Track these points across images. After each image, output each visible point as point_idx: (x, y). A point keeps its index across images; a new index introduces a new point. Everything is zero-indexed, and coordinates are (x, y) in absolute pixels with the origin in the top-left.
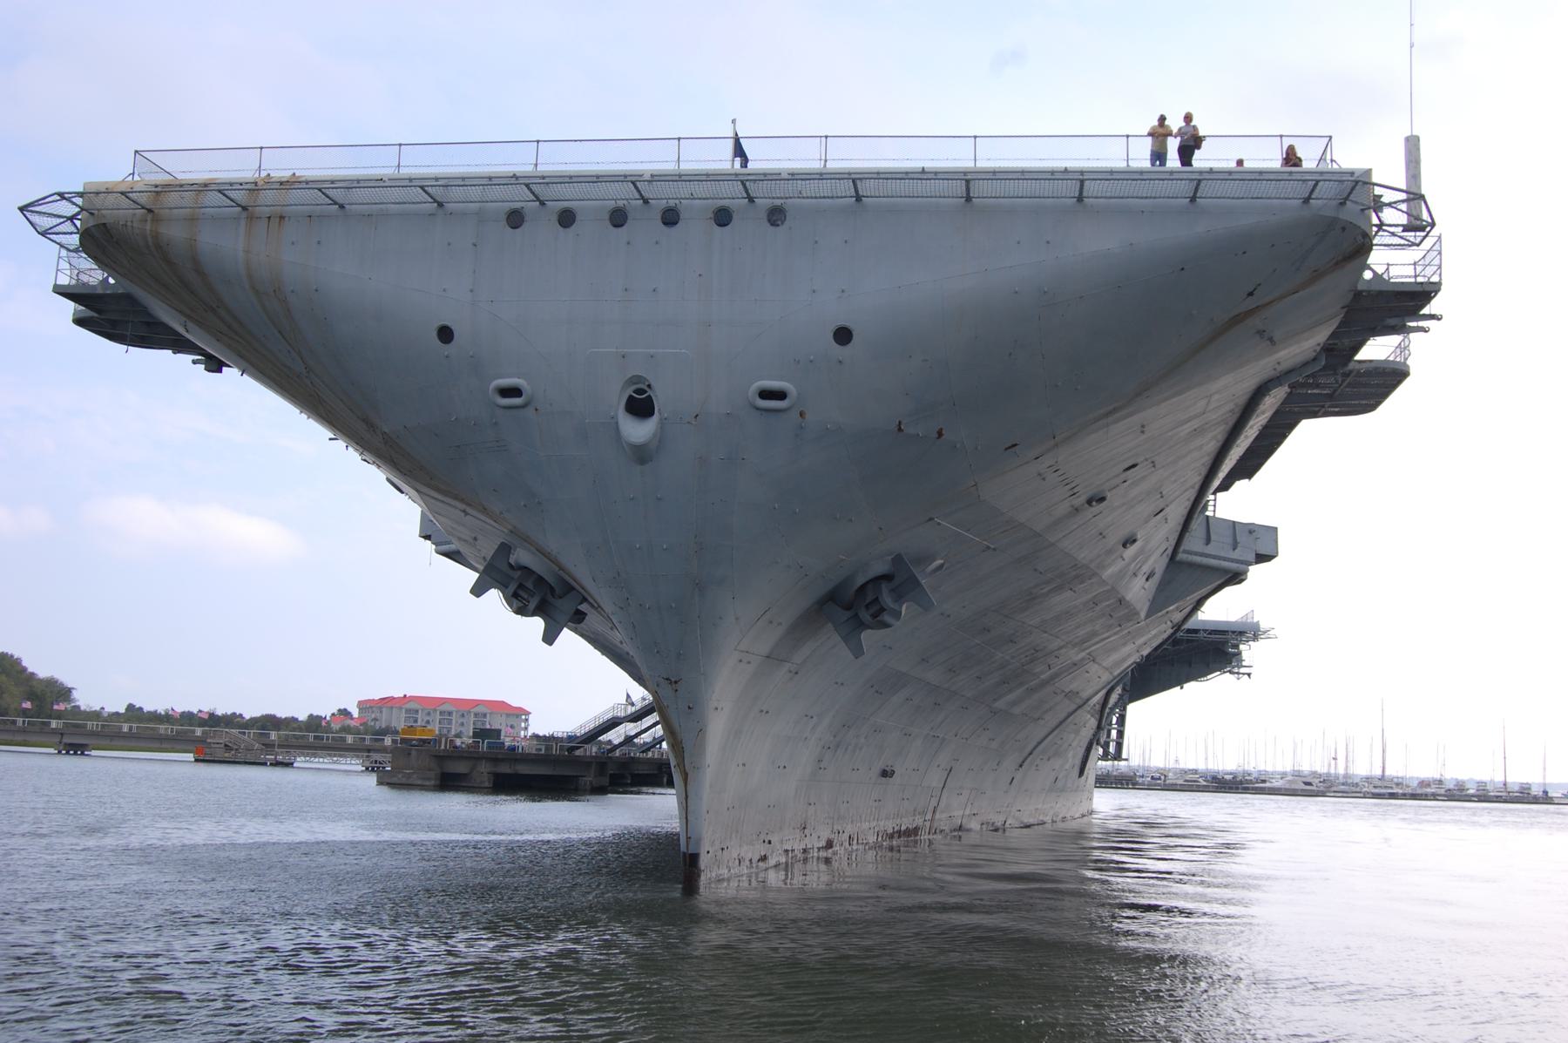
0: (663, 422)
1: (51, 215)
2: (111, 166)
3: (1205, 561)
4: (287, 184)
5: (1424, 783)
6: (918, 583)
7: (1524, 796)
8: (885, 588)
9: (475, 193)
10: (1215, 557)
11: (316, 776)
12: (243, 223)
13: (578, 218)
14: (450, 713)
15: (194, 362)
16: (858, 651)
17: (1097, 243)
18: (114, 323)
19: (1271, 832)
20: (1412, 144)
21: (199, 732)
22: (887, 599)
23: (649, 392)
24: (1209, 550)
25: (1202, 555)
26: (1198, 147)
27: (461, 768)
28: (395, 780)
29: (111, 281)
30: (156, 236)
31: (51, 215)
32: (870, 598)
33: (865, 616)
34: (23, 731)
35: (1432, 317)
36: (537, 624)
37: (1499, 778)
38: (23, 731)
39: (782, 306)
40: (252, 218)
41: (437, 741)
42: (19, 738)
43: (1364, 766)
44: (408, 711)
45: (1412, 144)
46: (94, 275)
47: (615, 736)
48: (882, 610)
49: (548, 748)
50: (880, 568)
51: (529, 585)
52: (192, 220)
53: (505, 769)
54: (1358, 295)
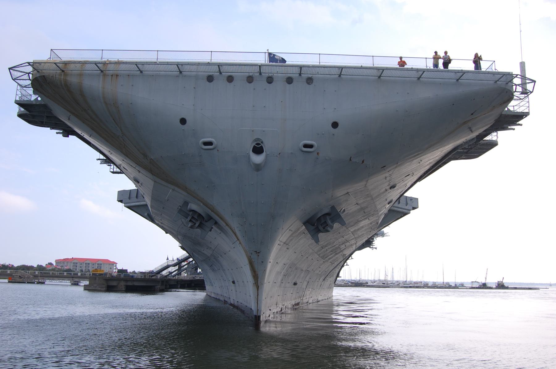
1: (21, 72)
2: (42, 55)
4: (118, 63)
5: (415, 283)
7: (448, 286)
8: (328, 218)
9: (194, 68)
11: (52, 287)
12: (101, 77)
13: (235, 79)
14: (89, 264)
15: (57, 133)
16: (317, 241)
17: (425, 94)
18: (33, 116)
21: (9, 272)
22: (329, 222)
23: (262, 145)
24: (400, 206)
25: (397, 207)
26: (450, 63)
27: (114, 283)
28: (90, 288)
29: (39, 99)
31: (21, 72)
32: (323, 221)
33: (321, 228)
35: (519, 125)
37: (442, 281)
39: (311, 115)
40: (105, 75)
41: (106, 274)
43: (399, 277)
44: (74, 263)
46: (32, 96)
47: (164, 273)
49: (145, 276)
50: (326, 211)
52: (81, 75)
53: (130, 284)
54: (501, 115)
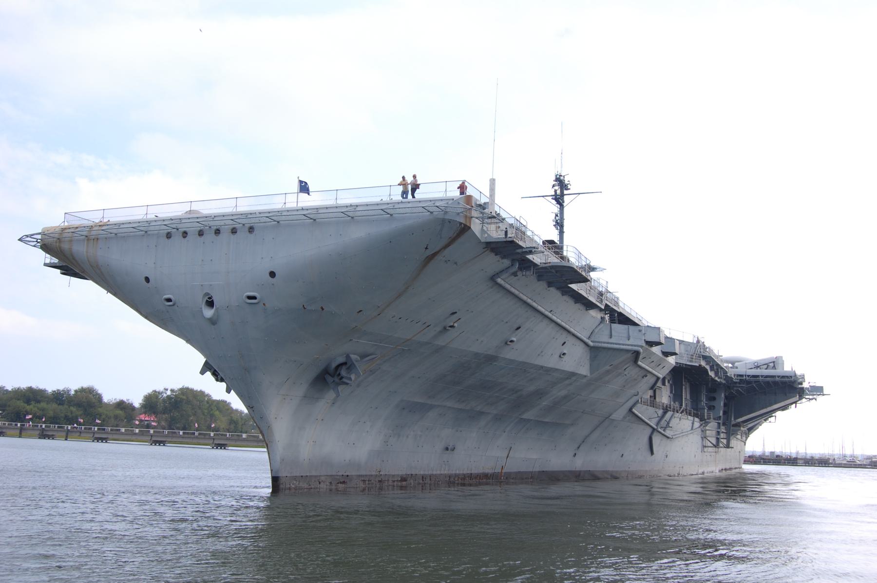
0: (217, 309)
8: (344, 367)
19: (809, 486)
20: (493, 182)
22: (343, 372)
24: (613, 340)
30: (60, 248)
42: (195, 441)
45: (493, 182)
48: (342, 378)
50: (341, 360)
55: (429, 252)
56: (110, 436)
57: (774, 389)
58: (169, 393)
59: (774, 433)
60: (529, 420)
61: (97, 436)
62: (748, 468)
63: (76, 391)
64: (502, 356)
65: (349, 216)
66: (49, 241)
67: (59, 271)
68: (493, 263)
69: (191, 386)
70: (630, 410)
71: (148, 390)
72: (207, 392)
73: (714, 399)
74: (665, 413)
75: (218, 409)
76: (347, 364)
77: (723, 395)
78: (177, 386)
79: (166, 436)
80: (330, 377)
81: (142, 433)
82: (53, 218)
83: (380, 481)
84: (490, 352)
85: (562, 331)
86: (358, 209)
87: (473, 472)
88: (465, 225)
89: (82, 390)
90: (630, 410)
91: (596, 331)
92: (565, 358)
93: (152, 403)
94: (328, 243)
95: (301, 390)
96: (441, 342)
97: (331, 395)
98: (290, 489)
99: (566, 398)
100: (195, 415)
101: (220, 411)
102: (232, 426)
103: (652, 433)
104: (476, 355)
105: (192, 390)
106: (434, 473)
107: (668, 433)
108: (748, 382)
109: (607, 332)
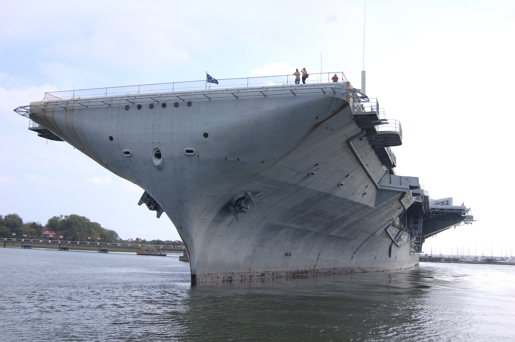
0: (163, 159)
3: (390, 189)
6: (251, 200)
8: (243, 201)
9: (118, 102)
10: (393, 187)
18: (49, 136)
19: (479, 277)
20: (363, 73)
22: (243, 204)
24: (391, 185)
25: (389, 187)
30: (45, 116)
34: (89, 246)
36: (155, 212)
38: (89, 246)
42: (88, 248)
45: (363, 73)
46: (37, 125)
48: (242, 207)
50: (241, 195)
51: (152, 202)
55: (318, 121)
56: (33, 245)
57: (451, 216)
58: (64, 218)
59: (435, 244)
60: (332, 236)
61: (24, 244)
62: (422, 264)
63: (6, 217)
64: (333, 194)
65: (264, 94)
66: (37, 111)
67: (37, 133)
68: (353, 129)
69: (77, 214)
70: (386, 230)
71: (51, 217)
72: (87, 217)
73: (417, 223)
74: (400, 231)
75: (94, 228)
76: (245, 199)
77: (422, 221)
78: (69, 214)
79: (69, 245)
80: (233, 207)
81: (53, 243)
82: (36, 95)
83: (250, 276)
84: (328, 192)
85: (369, 180)
86: (269, 90)
87: (299, 269)
88: (347, 102)
89: (10, 216)
90: (386, 230)
91: (383, 179)
92: (365, 196)
93: (53, 224)
94: (246, 114)
95: (211, 217)
96: (302, 185)
97: (230, 218)
98: (202, 282)
99: (356, 222)
100: (79, 231)
101: (95, 229)
102: (103, 239)
103: (392, 244)
104: (320, 193)
105: (78, 217)
106: (279, 270)
107: (399, 244)
108: (437, 213)
109: (388, 180)
